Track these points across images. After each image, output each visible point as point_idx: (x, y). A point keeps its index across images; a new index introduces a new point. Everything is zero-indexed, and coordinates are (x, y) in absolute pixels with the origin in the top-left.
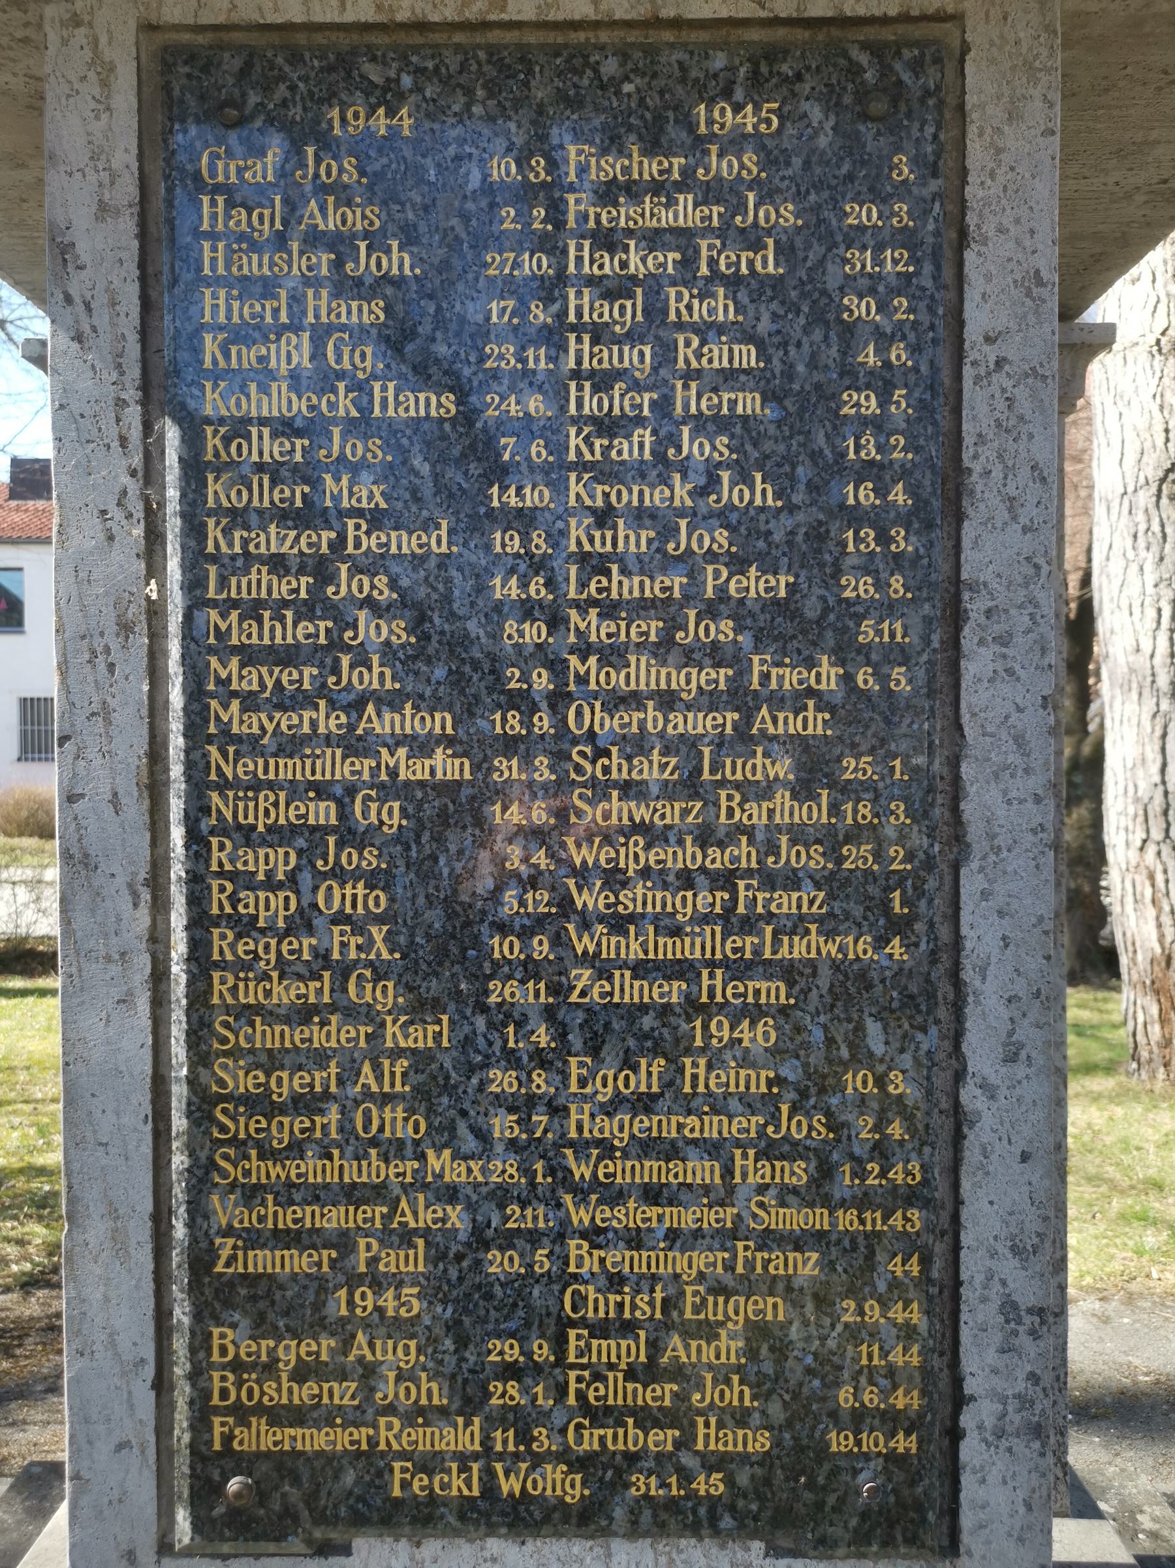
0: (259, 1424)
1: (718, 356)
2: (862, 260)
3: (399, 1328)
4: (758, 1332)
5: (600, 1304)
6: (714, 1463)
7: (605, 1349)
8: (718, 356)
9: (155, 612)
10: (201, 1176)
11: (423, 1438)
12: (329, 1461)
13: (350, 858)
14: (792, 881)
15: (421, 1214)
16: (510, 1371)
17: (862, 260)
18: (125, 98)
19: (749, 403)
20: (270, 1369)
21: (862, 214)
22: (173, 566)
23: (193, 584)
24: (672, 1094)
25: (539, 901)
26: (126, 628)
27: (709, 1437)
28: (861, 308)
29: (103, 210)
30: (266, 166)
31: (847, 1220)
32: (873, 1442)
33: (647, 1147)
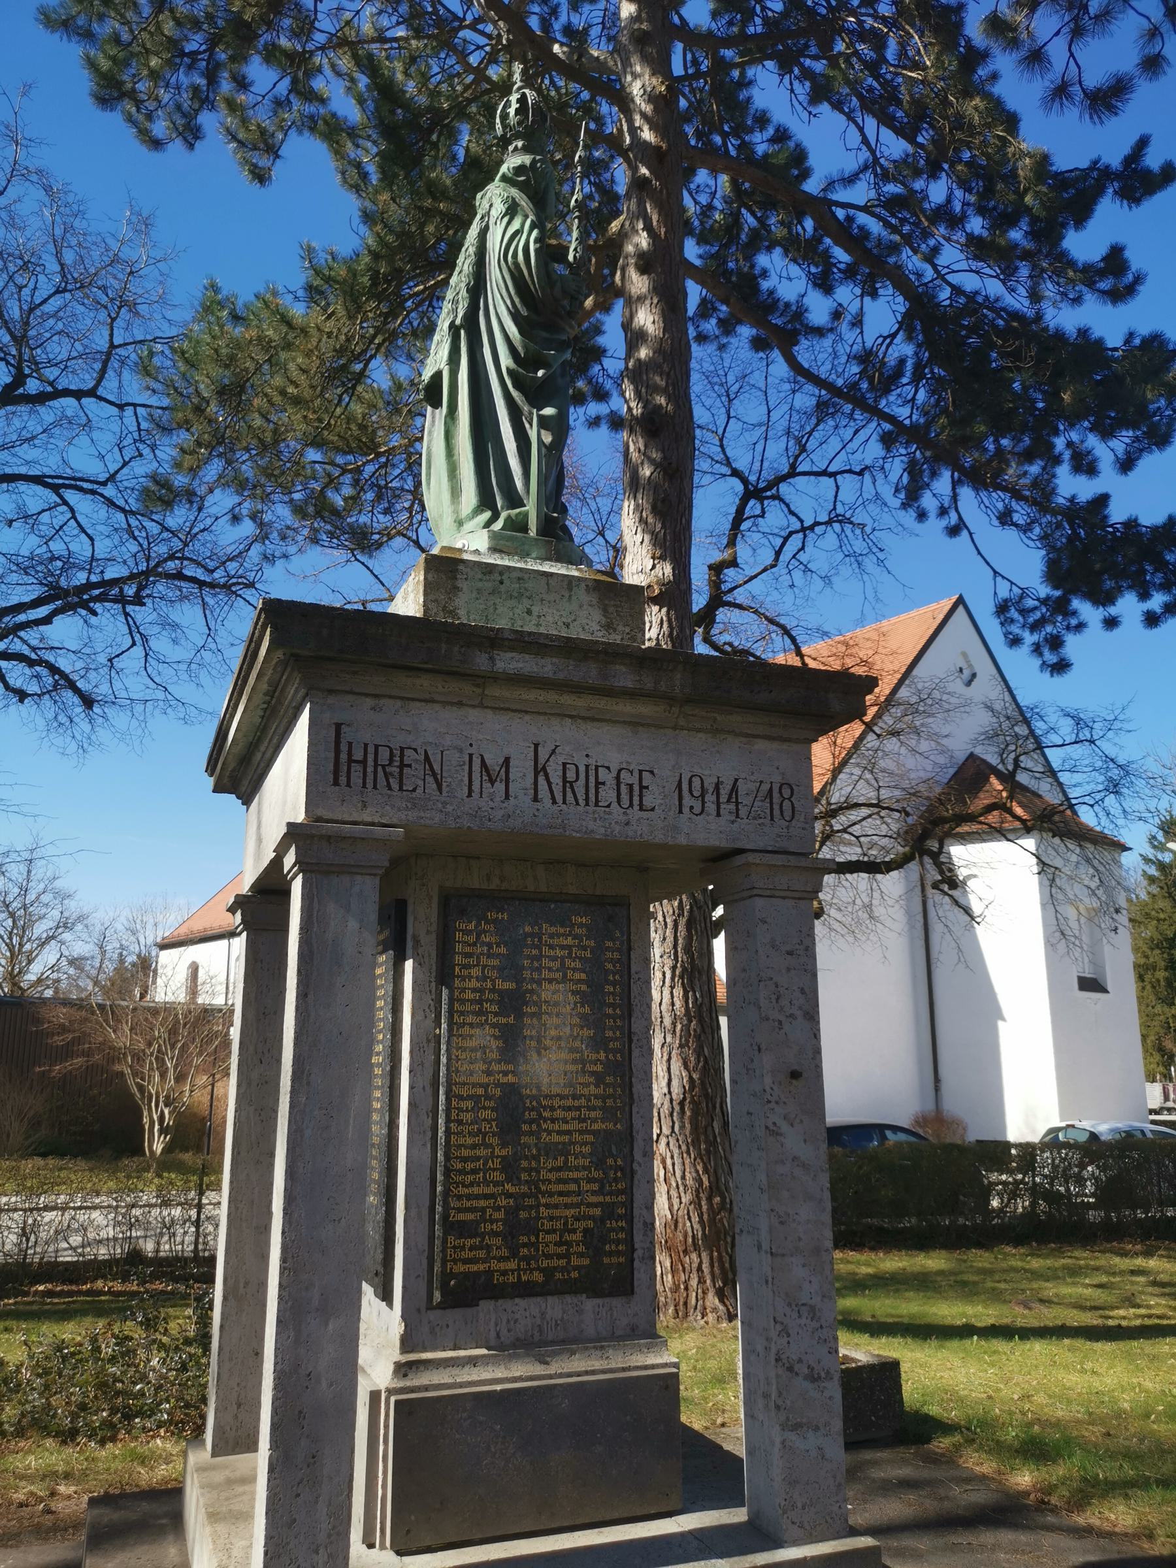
0: (460, 1264)
1: (577, 976)
2: (609, 955)
3: (495, 1234)
4: (586, 1231)
5: (548, 1225)
6: (575, 1268)
7: (549, 1238)
8: (577, 976)
9: (438, 1038)
10: (446, 1193)
11: (503, 1266)
12: (477, 1274)
13: (487, 1104)
14: (594, 1108)
15: (503, 1202)
16: (524, 1245)
17: (609, 955)
18: (435, 905)
19: (584, 987)
20: (463, 1248)
21: (609, 944)
22: (444, 1026)
23: (450, 1030)
24: (565, 1167)
25: (534, 1115)
26: (429, 1041)
27: (575, 1261)
28: (609, 966)
29: (428, 932)
30: (472, 926)
31: (608, 1199)
32: (614, 1260)
33: (560, 1181)
